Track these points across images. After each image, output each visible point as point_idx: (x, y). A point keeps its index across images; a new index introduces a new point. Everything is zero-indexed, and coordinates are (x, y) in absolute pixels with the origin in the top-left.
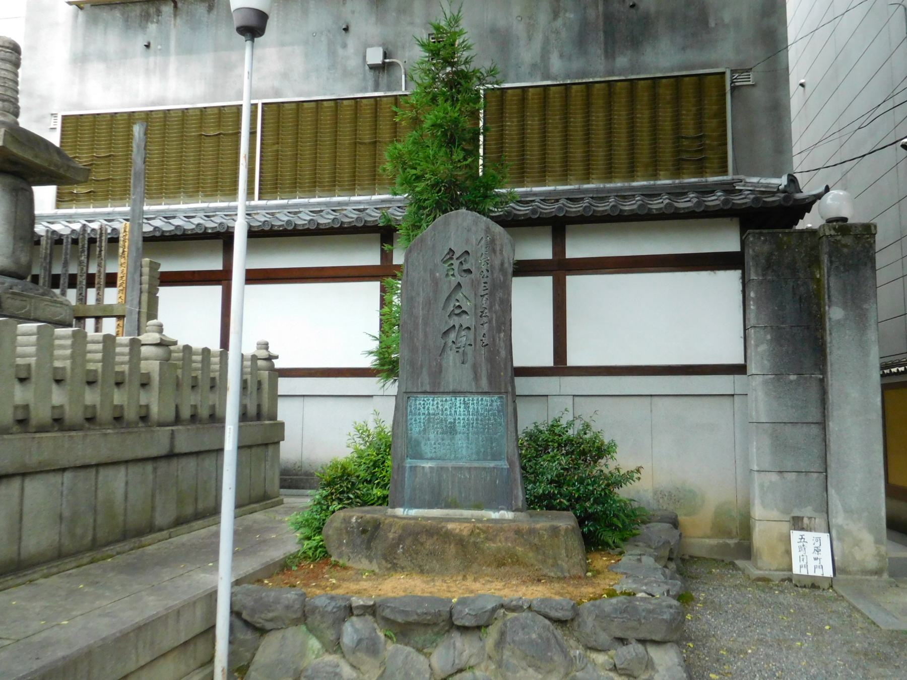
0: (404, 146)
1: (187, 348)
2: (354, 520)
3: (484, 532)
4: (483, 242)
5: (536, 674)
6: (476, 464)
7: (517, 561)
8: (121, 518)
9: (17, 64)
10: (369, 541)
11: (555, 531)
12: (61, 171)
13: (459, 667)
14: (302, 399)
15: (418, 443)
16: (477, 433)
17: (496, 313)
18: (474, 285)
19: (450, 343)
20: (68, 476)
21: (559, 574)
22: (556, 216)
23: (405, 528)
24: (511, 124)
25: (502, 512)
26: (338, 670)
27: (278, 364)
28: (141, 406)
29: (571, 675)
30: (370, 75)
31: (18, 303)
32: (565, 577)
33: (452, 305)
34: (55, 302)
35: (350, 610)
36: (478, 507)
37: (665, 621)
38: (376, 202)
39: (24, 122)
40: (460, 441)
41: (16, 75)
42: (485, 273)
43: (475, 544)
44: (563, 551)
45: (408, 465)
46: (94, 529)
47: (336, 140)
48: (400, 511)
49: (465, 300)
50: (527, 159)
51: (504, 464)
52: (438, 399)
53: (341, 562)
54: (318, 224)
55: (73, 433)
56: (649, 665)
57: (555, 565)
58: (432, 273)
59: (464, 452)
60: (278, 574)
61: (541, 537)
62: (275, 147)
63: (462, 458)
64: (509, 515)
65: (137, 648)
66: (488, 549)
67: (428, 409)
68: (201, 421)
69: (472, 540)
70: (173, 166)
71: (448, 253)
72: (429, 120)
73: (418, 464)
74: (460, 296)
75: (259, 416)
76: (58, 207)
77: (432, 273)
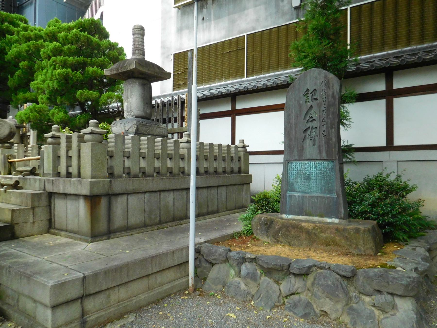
0: (300, 42)
1: (211, 145)
2: (263, 219)
3: (320, 228)
4: (323, 84)
5: (330, 302)
6: (320, 195)
7: (336, 244)
8: (172, 213)
9: (143, 35)
10: (268, 228)
11: (357, 231)
12: (159, 75)
13: (292, 292)
14: (264, 164)
15: (293, 184)
16: (321, 180)
17: (330, 119)
18: (319, 106)
19: (308, 136)
20: (147, 195)
21: (358, 252)
22: (385, 67)
23: (282, 224)
24: (365, 23)
25: (333, 219)
26: (239, 285)
27: (248, 149)
28: (180, 168)
29: (350, 305)
30: (294, 12)
31: (145, 128)
32: (362, 254)
33: (308, 116)
34: (160, 127)
35: (244, 260)
36: (321, 216)
37: (403, 285)
38: (295, 72)
39: (148, 58)
40: (313, 183)
41: (143, 39)
42: (324, 99)
43: (315, 234)
44: (362, 241)
45: (288, 195)
46: (160, 216)
47: (278, 46)
48: (284, 216)
49: (315, 114)
50: (374, 40)
51: (334, 195)
52: (302, 163)
53: (257, 237)
54: (267, 85)
55: (148, 178)
56: (394, 307)
57: (357, 247)
58: (298, 102)
59: (315, 189)
60: (228, 240)
61: (350, 233)
62: (253, 53)
63: (314, 192)
64: (336, 221)
65: (152, 265)
66: (322, 237)
68: (210, 174)
69: (314, 231)
70: (213, 68)
71: (306, 91)
72: (310, 26)
73: (293, 194)
74: (312, 112)
75: (240, 172)
76: (174, 91)
77: (298, 102)
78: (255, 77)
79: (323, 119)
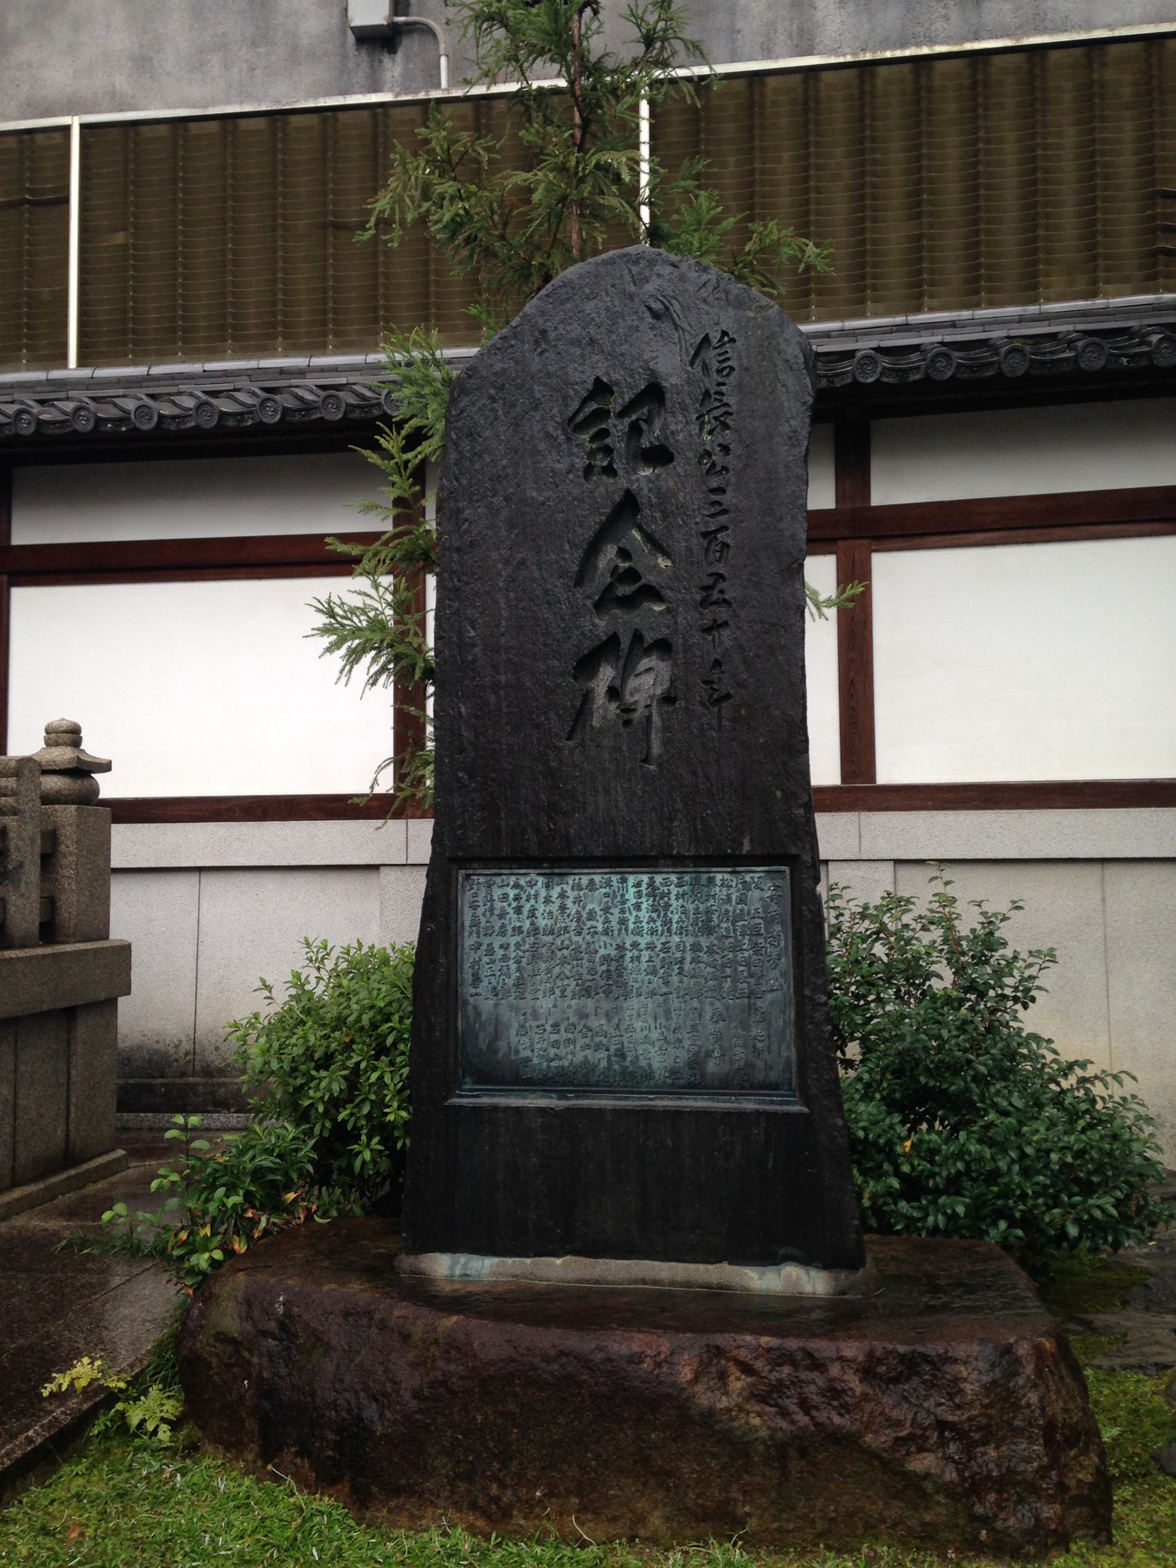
27: (109, 787)
67: (532, 914)
71: (591, 396)
78: (141, 371)
79: (708, 588)
